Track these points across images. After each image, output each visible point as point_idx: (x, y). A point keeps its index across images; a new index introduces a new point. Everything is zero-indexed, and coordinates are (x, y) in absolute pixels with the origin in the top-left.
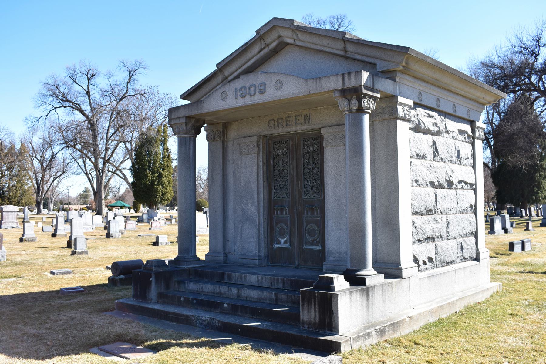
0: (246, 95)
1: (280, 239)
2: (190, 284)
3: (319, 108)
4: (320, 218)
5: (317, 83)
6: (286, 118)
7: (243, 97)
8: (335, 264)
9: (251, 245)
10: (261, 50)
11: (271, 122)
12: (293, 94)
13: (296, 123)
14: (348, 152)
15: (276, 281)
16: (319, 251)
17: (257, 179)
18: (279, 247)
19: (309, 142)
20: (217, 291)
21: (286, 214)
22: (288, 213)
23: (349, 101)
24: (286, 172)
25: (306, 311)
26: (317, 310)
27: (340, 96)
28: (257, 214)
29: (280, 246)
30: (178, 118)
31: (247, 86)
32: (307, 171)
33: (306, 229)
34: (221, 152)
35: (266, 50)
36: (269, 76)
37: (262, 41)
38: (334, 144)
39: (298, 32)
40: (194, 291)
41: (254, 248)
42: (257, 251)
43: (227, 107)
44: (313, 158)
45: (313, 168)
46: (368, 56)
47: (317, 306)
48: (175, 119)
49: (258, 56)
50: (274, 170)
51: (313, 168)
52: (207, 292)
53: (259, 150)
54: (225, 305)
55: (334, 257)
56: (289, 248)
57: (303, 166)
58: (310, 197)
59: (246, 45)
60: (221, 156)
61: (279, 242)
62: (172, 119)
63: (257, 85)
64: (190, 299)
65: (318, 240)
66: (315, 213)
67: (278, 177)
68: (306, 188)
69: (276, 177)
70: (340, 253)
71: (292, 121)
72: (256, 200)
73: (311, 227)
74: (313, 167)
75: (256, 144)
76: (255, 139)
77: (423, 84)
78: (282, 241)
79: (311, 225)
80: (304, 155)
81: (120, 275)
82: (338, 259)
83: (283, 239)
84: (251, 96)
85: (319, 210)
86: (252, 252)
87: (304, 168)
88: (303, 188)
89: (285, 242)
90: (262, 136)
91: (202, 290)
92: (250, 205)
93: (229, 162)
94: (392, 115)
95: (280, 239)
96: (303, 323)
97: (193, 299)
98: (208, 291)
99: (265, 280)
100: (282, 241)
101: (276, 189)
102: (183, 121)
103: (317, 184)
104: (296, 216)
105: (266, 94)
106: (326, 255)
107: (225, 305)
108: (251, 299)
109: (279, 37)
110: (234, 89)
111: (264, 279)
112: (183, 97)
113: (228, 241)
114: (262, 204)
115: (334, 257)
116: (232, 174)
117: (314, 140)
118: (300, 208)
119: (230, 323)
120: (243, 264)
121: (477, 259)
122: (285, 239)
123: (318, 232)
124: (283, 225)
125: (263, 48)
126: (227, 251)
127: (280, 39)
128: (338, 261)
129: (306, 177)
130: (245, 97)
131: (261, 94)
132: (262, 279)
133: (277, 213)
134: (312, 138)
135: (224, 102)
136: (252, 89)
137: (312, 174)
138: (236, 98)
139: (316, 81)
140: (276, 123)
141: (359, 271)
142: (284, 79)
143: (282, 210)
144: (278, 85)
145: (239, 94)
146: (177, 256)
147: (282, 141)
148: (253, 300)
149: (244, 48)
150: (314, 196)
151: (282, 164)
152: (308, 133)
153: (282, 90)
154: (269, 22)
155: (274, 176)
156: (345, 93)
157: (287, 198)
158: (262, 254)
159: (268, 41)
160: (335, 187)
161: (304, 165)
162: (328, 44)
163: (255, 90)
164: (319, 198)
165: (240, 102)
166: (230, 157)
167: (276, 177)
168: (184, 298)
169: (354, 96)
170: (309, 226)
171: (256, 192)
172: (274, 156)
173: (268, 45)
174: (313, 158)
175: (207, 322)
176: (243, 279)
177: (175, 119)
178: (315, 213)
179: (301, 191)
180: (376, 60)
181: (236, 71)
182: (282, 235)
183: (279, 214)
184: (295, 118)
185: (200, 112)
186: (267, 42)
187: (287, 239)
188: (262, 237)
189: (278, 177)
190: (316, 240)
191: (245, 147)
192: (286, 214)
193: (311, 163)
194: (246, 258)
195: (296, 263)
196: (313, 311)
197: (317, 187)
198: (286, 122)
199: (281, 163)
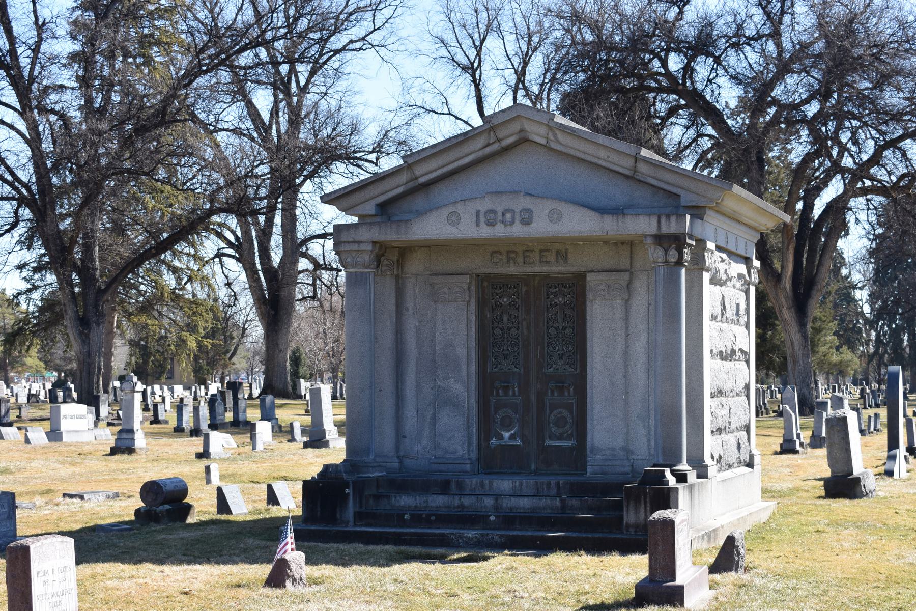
1: (503, 433)
2: (401, 497)
7: (491, 224)
10: (488, 145)
11: (494, 255)
12: (580, 232)
14: (661, 316)
15: (545, 486)
16: (572, 447)
18: (500, 445)
19: (557, 289)
20: (456, 504)
21: (514, 394)
22: (517, 393)
23: (666, 251)
24: (514, 331)
25: (632, 512)
26: (648, 508)
27: (654, 243)
29: (502, 442)
30: (354, 242)
31: (499, 209)
32: (552, 331)
34: (393, 295)
35: (495, 147)
36: (539, 201)
37: (492, 133)
38: (607, 297)
39: (557, 132)
40: (409, 507)
43: (459, 235)
45: (564, 328)
46: (668, 183)
47: (648, 505)
48: (349, 243)
51: (564, 328)
52: (437, 507)
53: (470, 297)
54: (492, 518)
60: (393, 301)
61: (501, 437)
62: (342, 242)
63: (517, 211)
64: (424, 516)
65: (569, 432)
66: (566, 394)
70: (613, 449)
71: (536, 256)
72: (464, 373)
73: (560, 413)
75: (466, 287)
77: (727, 221)
78: (506, 435)
80: (548, 309)
81: (163, 503)
82: (610, 457)
83: (508, 431)
84: (506, 225)
85: (572, 389)
87: (548, 328)
89: (512, 437)
91: (425, 505)
92: (452, 381)
94: (697, 264)
96: (628, 526)
97: (429, 516)
98: (438, 504)
99: (527, 487)
100: (506, 435)
103: (570, 351)
105: (533, 225)
107: (492, 518)
108: (519, 511)
109: (521, 131)
111: (524, 484)
112: (327, 199)
113: (404, 437)
116: (414, 330)
117: (565, 287)
118: (539, 386)
120: (440, 472)
121: (750, 465)
122: (512, 432)
124: (510, 411)
126: (402, 453)
128: (610, 460)
130: (494, 225)
131: (523, 224)
132: (521, 484)
133: (498, 394)
134: (562, 284)
135: (454, 229)
136: (508, 216)
138: (478, 225)
139: (617, 219)
140: (505, 259)
141: (675, 465)
142: (565, 208)
143: (506, 389)
144: (556, 217)
145: (482, 219)
147: (507, 285)
148: (522, 511)
149: (460, 139)
153: (561, 223)
156: (660, 239)
157: (516, 370)
158: (474, 456)
159: (501, 133)
161: (548, 323)
162: (608, 157)
163: (513, 218)
165: (485, 232)
166: (409, 303)
168: (411, 515)
169: (674, 246)
173: (499, 140)
175: (475, 540)
176: (487, 487)
177: (349, 243)
178: (566, 394)
180: (679, 190)
181: (435, 170)
183: (501, 394)
185: (403, 237)
186: (500, 135)
187: (515, 433)
191: (445, 290)
192: (514, 394)
193: (560, 320)
194: (447, 462)
195: (533, 467)
196: (642, 510)
198: (524, 257)
199: (505, 318)
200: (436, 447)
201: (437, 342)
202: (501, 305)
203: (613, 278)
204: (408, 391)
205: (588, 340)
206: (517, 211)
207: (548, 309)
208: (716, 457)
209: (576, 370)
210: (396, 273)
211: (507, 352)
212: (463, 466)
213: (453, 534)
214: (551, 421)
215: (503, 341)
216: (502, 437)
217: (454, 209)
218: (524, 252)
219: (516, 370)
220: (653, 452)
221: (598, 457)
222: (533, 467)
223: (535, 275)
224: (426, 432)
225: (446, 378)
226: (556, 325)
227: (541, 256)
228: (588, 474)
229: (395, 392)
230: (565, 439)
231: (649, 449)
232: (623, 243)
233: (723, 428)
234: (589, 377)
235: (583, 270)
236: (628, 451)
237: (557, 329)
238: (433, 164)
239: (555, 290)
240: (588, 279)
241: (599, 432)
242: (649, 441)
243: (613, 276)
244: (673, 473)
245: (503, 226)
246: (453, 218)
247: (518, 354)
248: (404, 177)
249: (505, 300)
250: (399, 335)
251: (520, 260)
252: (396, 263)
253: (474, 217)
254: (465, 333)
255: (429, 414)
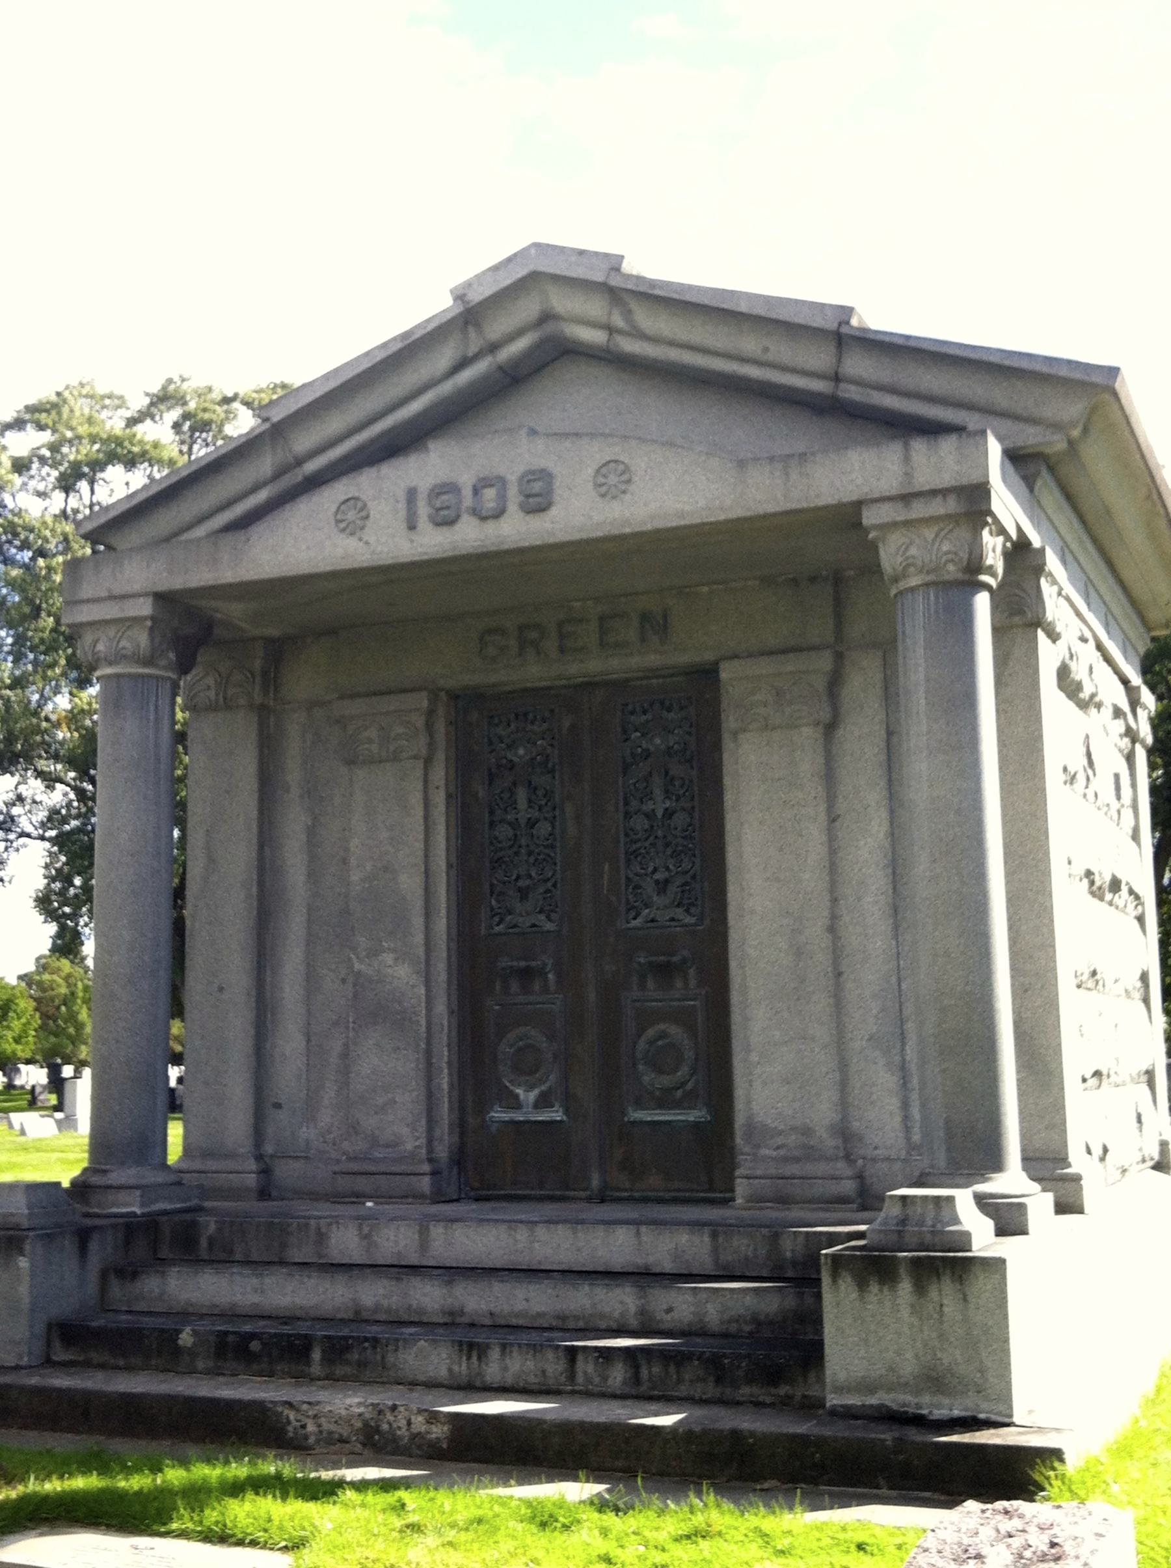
0: (458, 517)
3: (705, 589)
4: (697, 1003)
5: (787, 474)
6: (560, 625)
7: (444, 520)
8: (788, 1174)
9: (391, 1118)
12: (681, 514)
13: (602, 644)
16: (696, 1125)
17: (426, 856)
19: (649, 716)
22: (552, 987)
24: (543, 829)
28: (422, 991)
30: (112, 597)
31: (466, 480)
33: (635, 1044)
36: (568, 444)
39: (633, 305)
41: (405, 1131)
42: (423, 1141)
44: (667, 773)
45: (669, 814)
49: (447, 388)
50: (492, 824)
53: (431, 745)
55: (778, 1148)
56: (561, 1122)
57: (621, 804)
58: (653, 921)
59: (402, 341)
63: (512, 478)
65: (689, 1086)
67: (511, 847)
68: (637, 887)
69: (501, 849)
72: (419, 938)
73: (663, 1035)
74: (666, 809)
75: (420, 722)
76: (422, 701)
78: (528, 1096)
79: (662, 1026)
82: (796, 1153)
83: (531, 1087)
86: (397, 1145)
87: (627, 815)
88: (623, 888)
89: (543, 1102)
90: (443, 694)
92: (389, 958)
93: (288, 791)
94: (1021, 612)
95: (519, 1091)
100: (528, 1096)
101: (501, 893)
102: (145, 608)
104: (592, 997)
105: (554, 511)
106: (738, 1140)
109: (546, 317)
110: (402, 495)
113: (278, 1106)
114: (445, 955)
115: (778, 1148)
119: (604, 1423)
123: (689, 1054)
124: (533, 1033)
125: (470, 354)
126: (269, 1149)
127: (549, 328)
129: (634, 847)
131: (528, 512)
134: (662, 703)
137: (660, 833)
138: (412, 527)
140: (513, 642)
145: (423, 510)
146: (85, 1170)
150: (673, 919)
151: (530, 801)
152: (645, 682)
154: (509, 260)
155: (491, 843)
157: (549, 926)
158: (442, 1152)
160: (778, 880)
161: (626, 803)
164: (696, 925)
167: (501, 849)
170: (651, 1032)
171: (419, 904)
172: (490, 770)
173: (493, 348)
174: (667, 773)
179: (613, 899)
182: (527, 1069)
184: (601, 627)
188: (444, 1081)
189: (511, 847)
190: (683, 1084)
191: (372, 733)
192: (545, 990)
193: (658, 793)
194: (372, 1168)
195: (595, 1182)
197: (686, 884)
199: (522, 795)
200: (354, 1128)
201: (353, 861)
202: (512, 766)
203: (790, 668)
204: (287, 989)
205: (730, 838)
206: (512, 478)
207: (626, 768)
208: (1097, 1151)
209: (701, 920)
210: (258, 699)
211: (528, 882)
212: (414, 1179)
213: (290, 1405)
214: (639, 1055)
215: (517, 854)
216: (516, 1104)
217: (353, 492)
218: (560, 625)
219: (549, 926)
220: (916, 1138)
221: (765, 1152)
222: (595, 1182)
223: (590, 686)
224: (329, 1094)
225: (374, 953)
226: (648, 806)
227: (603, 631)
228: (739, 1201)
229: (254, 993)
230: (677, 1105)
231: (908, 1130)
232: (813, 579)
233: (1105, 1072)
234: (734, 937)
235: (709, 656)
236: (846, 1134)
237: (650, 816)
238: (334, 424)
239: (644, 718)
240: (724, 676)
241: (765, 1083)
242: (905, 1106)
243: (791, 664)
244: (984, 1203)
245: (474, 521)
246: (351, 515)
247: (554, 885)
248: (265, 465)
249: (521, 752)
250: (267, 850)
251: (551, 645)
252: (258, 680)
253: (402, 506)
254: (422, 837)
255: (337, 1046)
